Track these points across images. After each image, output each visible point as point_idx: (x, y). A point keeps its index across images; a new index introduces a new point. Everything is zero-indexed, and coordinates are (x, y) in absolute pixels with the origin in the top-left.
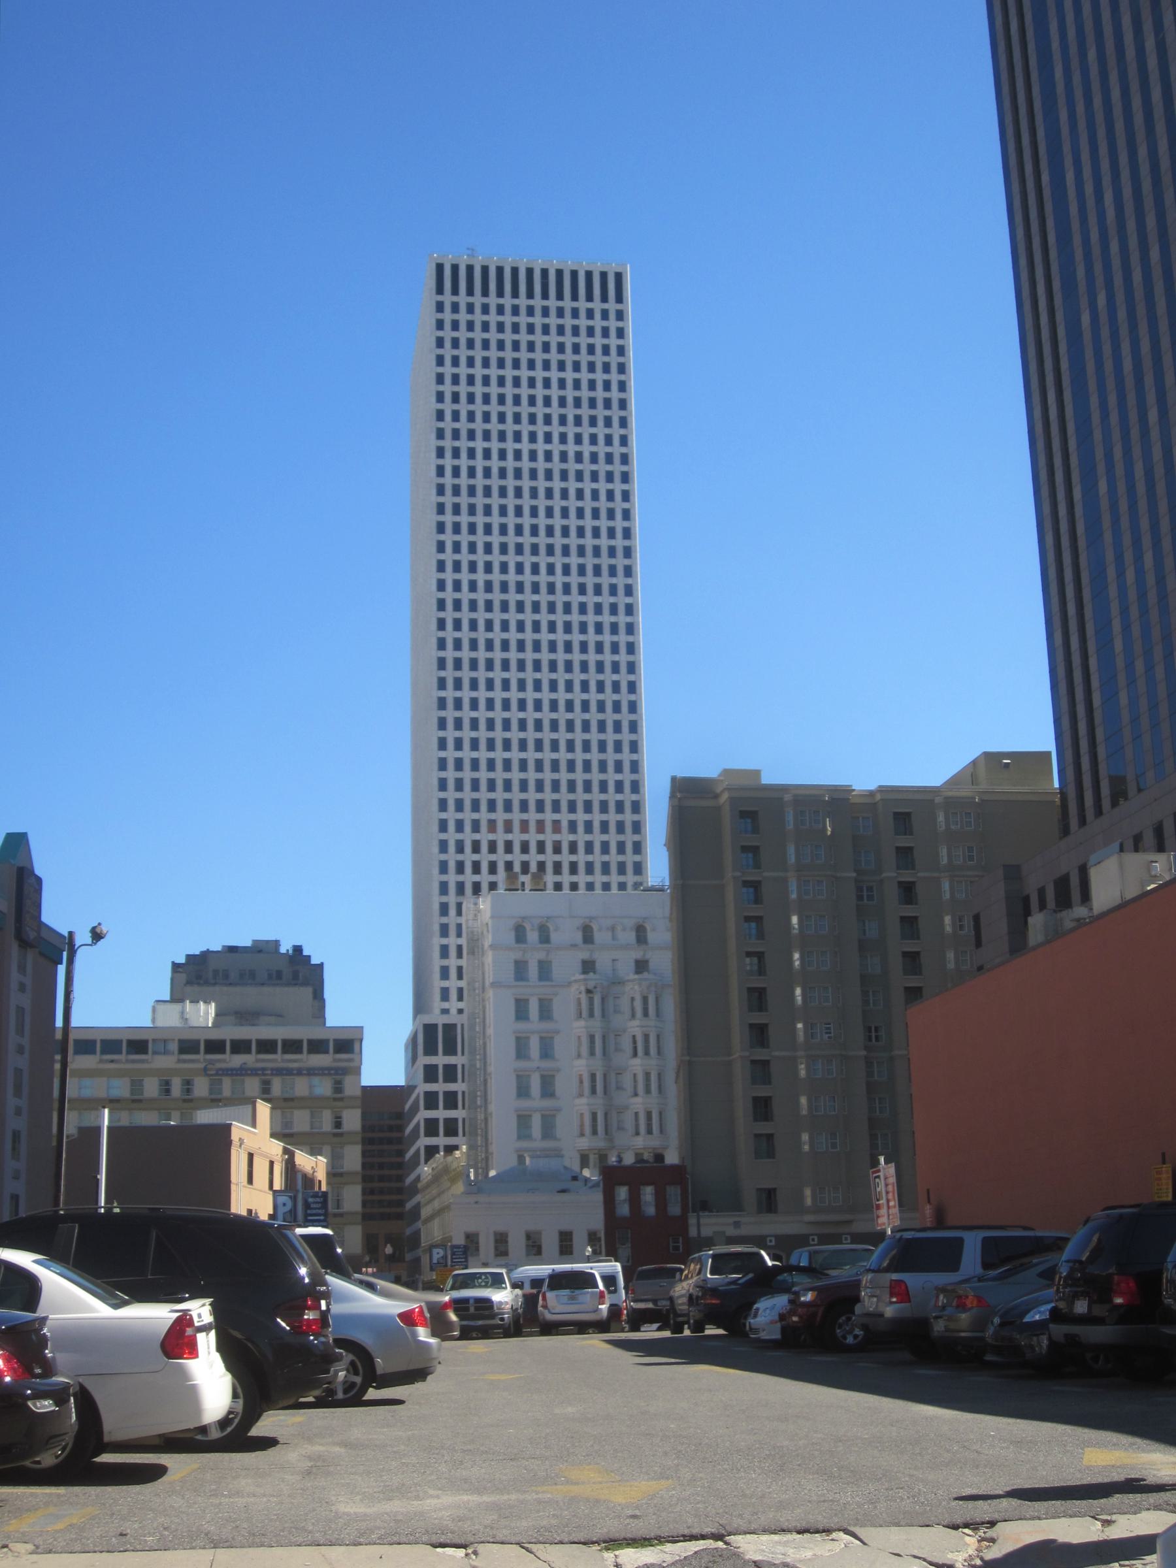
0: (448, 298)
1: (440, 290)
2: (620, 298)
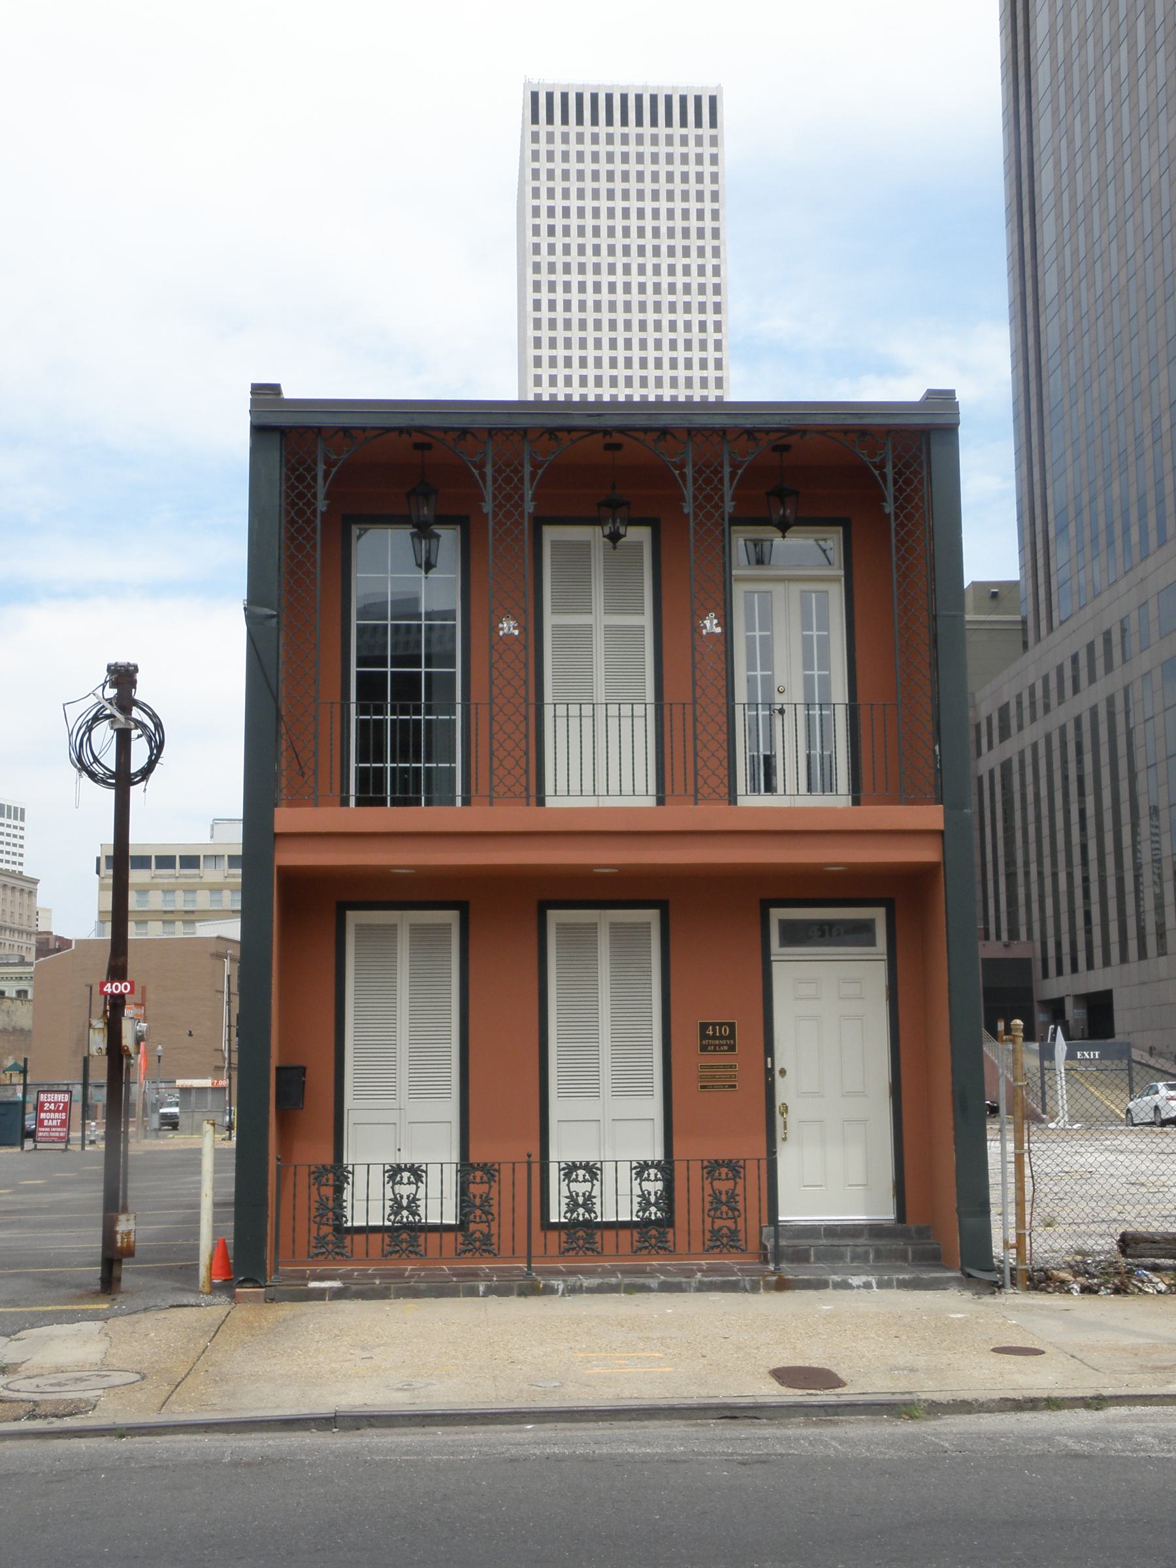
0: (543, 128)
1: (535, 120)
2: (713, 124)
